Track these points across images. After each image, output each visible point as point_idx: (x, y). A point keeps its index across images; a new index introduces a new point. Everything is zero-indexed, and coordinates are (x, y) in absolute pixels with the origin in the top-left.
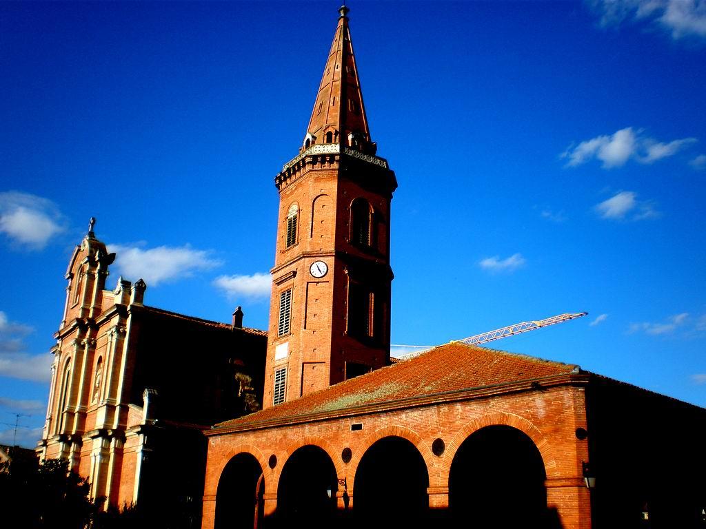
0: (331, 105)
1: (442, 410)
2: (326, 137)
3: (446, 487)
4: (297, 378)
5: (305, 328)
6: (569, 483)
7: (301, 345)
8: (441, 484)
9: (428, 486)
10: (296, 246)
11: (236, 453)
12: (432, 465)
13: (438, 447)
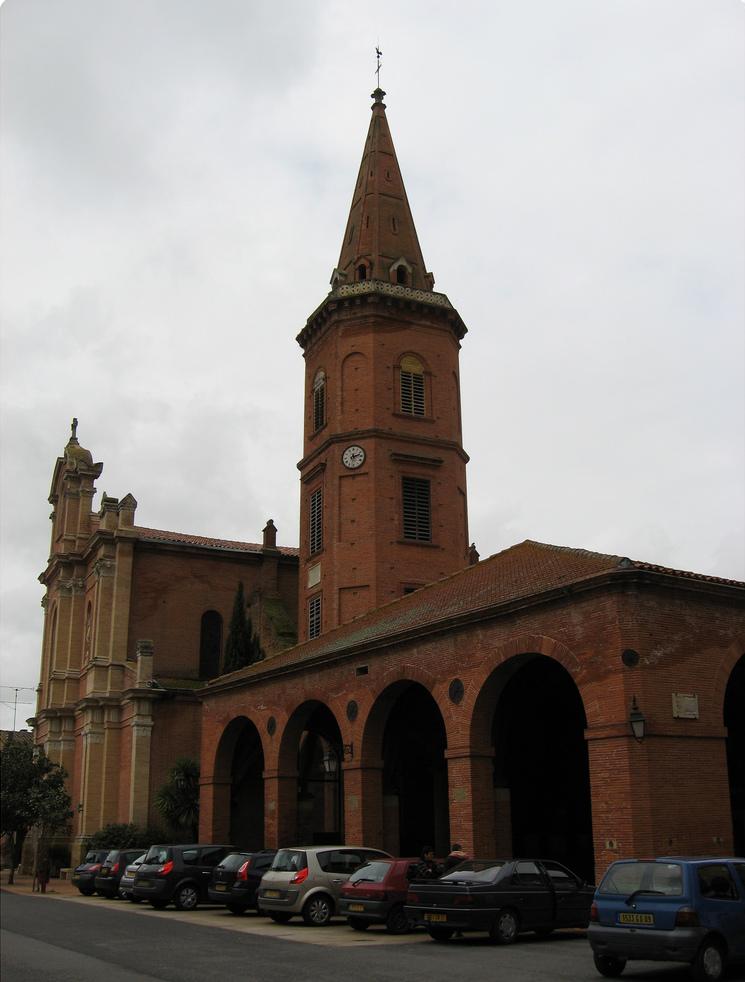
0: (364, 227)
1: (459, 639)
2: (357, 272)
3: (467, 747)
4: (334, 609)
5: (340, 541)
6: (614, 732)
7: (336, 563)
8: (461, 743)
9: (445, 747)
10: (324, 428)
11: (330, 706)
12: (450, 717)
13: (456, 692)
